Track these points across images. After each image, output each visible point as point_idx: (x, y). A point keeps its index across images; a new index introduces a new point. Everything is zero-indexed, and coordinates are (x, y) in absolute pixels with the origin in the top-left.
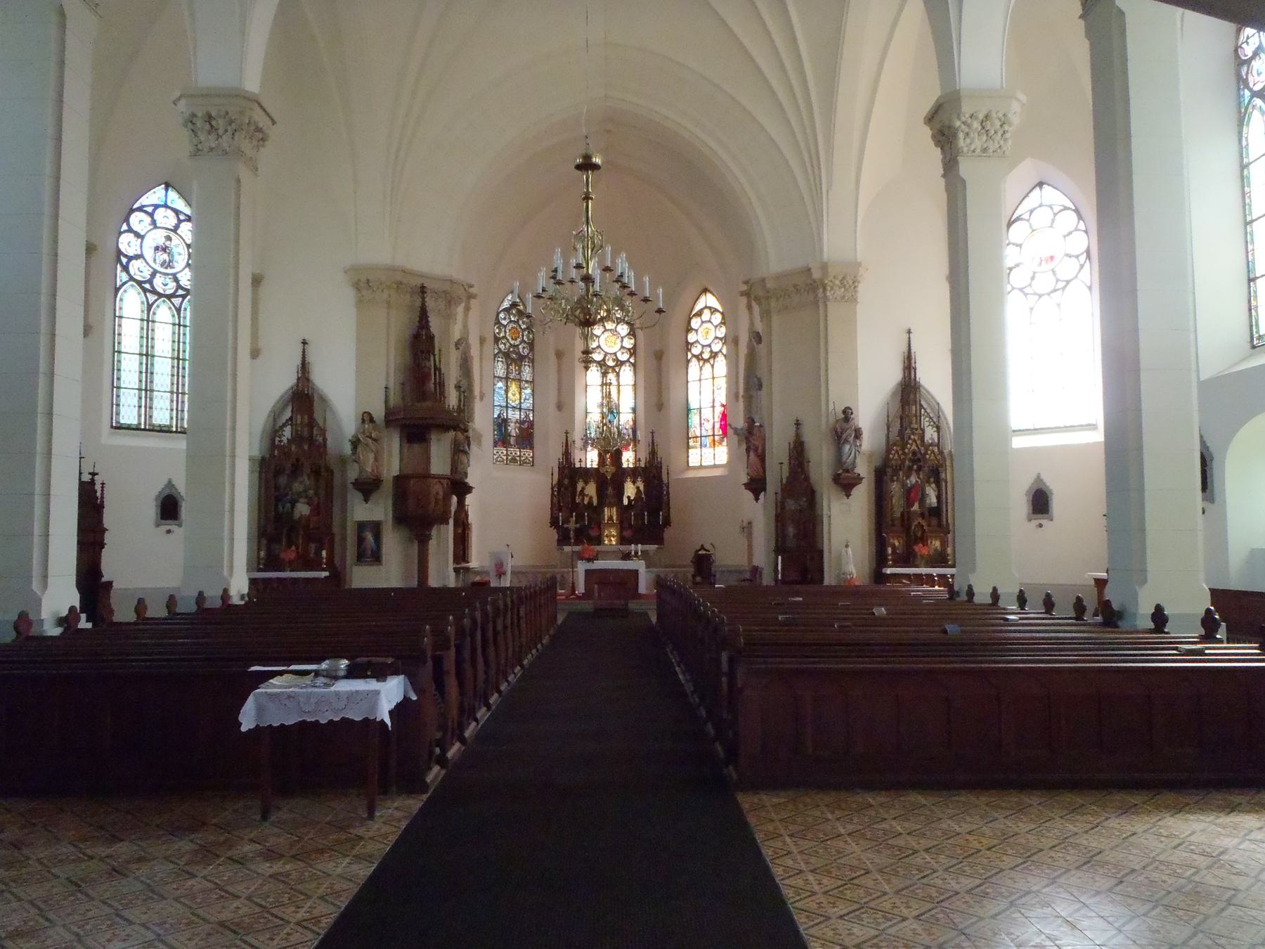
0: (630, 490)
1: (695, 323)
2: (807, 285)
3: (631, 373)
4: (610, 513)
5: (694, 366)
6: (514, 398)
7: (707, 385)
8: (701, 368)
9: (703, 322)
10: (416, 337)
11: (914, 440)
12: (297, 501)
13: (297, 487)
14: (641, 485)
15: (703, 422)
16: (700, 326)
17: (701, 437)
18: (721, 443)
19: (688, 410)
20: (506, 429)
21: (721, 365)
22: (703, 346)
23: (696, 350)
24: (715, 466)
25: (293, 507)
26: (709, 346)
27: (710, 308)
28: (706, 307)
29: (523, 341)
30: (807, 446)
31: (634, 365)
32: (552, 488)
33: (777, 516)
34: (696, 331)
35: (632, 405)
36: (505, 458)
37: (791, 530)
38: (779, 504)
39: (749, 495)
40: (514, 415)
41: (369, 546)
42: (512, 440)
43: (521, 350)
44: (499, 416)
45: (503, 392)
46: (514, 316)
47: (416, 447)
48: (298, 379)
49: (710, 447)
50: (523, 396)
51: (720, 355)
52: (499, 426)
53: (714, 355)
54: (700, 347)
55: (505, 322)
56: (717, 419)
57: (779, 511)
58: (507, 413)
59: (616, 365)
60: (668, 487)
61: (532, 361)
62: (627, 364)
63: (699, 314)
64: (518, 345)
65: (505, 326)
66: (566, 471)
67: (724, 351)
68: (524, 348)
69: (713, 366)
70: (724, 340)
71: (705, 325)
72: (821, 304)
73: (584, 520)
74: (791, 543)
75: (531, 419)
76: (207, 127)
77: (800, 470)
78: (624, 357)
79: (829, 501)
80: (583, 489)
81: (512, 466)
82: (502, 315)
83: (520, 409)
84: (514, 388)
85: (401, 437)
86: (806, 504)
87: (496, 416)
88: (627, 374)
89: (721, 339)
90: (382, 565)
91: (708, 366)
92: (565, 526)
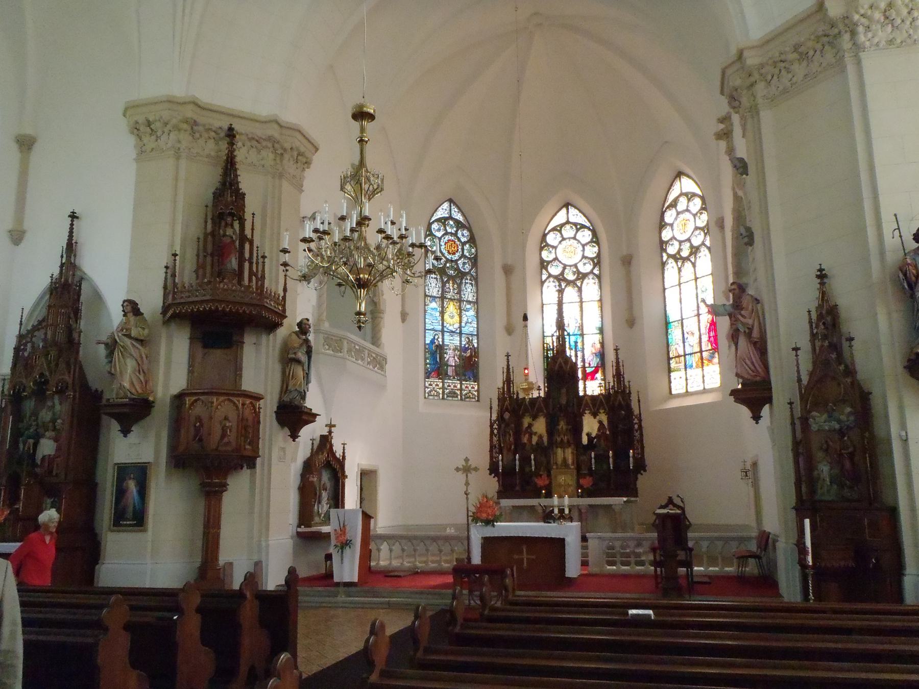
0: (590, 425)
1: (669, 216)
2: (818, 39)
3: (597, 287)
4: (563, 455)
5: (671, 268)
6: (452, 322)
7: (689, 289)
8: (680, 270)
9: (678, 213)
10: (218, 195)
12: (43, 436)
13: (45, 415)
14: (604, 418)
15: (686, 336)
16: (676, 219)
17: (685, 355)
18: (710, 361)
19: (667, 324)
20: (442, 358)
21: (705, 261)
22: (681, 242)
23: (672, 250)
24: (705, 391)
25: (36, 445)
26: (689, 240)
27: (686, 194)
28: (681, 194)
29: (463, 256)
30: (843, 313)
31: (599, 277)
32: (491, 426)
33: (796, 444)
34: (671, 225)
35: (599, 325)
36: (441, 391)
37: (824, 470)
38: (797, 422)
39: (744, 412)
40: (452, 342)
41: (130, 501)
42: (450, 371)
43: (461, 266)
44: (432, 342)
45: (438, 314)
46: (452, 227)
47: (218, 355)
48: (62, 265)
49: (697, 367)
50: (464, 319)
51: (703, 249)
52: (433, 354)
53: (695, 250)
54: (676, 244)
55: (439, 234)
56: (704, 330)
57: (799, 435)
58: (443, 339)
59: (577, 279)
60: (640, 420)
61: (476, 279)
62: (591, 276)
63: (674, 204)
64: (456, 261)
65: (440, 239)
66: (507, 403)
67: (708, 243)
68: (464, 264)
69: (694, 265)
70: (706, 230)
71: (682, 216)
73: (531, 467)
74: (827, 491)
75: (476, 345)
76: (148, 130)
77: (834, 356)
78: (586, 268)
79: (901, 408)
80: (530, 426)
81: (455, 402)
82: (435, 226)
83: (461, 334)
84: (451, 308)
85: (192, 339)
86: (852, 418)
87: (428, 342)
88: (591, 288)
89: (702, 229)
90: (145, 531)
91: (688, 265)
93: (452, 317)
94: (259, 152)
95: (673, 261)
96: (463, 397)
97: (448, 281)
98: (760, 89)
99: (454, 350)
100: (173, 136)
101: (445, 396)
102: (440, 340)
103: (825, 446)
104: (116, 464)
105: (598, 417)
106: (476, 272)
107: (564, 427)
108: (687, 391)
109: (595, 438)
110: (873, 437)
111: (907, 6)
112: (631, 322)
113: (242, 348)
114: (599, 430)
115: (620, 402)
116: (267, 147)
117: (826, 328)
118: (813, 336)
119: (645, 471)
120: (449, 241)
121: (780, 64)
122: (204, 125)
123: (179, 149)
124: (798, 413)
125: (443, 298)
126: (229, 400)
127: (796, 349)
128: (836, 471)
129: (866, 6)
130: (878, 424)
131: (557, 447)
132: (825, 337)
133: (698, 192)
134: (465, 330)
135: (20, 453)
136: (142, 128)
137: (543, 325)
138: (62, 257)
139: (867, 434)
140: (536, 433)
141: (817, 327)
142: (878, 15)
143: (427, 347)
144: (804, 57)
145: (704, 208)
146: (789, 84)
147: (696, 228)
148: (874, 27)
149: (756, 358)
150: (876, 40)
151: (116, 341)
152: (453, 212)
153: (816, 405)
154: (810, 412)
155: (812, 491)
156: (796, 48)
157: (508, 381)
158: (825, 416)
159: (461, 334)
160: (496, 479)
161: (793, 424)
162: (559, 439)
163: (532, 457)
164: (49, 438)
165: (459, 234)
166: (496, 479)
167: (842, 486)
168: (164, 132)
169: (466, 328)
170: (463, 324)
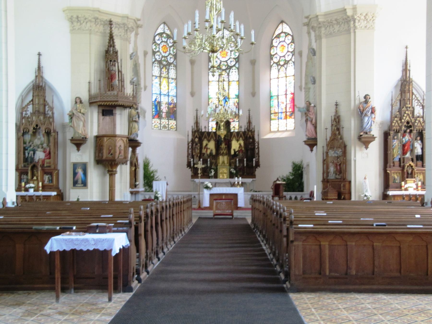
0: (235, 145)
4: (223, 159)
6: (164, 90)
8: (279, 70)
11: (408, 114)
13: (37, 142)
14: (242, 142)
15: (280, 103)
20: (160, 108)
21: (291, 69)
23: (275, 60)
24: (286, 130)
27: (285, 33)
30: (342, 118)
31: (238, 69)
32: (188, 144)
33: (324, 161)
37: (332, 169)
39: (308, 148)
40: (164, 100)
42: (164, 115)
44: (156, 100)
46: (165, 38)
47: (108, 118)
49: (284, 119)
51: (291, 62)
52: (156, 106)
53: (286, 62)
55: (159, 42)
56: (288, 102)
57: (325, 158)
61: (176, 66)
62: (234, 68)
63: (278, 36)
64: (167, 57)
65: (159, 45)
67: (293, 60)
70: (293, 53)
72: (352, 31)
76: (76, 20)
80: (207, 145)
83: (168, 96)
84: (164, 82)
85: (389, 191)
86: (341, 153)
87: (154, 100)
88: (234, 75)
90: (87, 188)
91: (283, 68)
92: (409, 125)
93: (165, 87)
94: (118, 29)
95: (276, 65)
96: (169, 128)
97: (163, 68)
98: (323, 29)
99: (166, 104)
100: (89, 24)
101: (161, 128)
102: (159, 99)
103: (332, 162)
104: (72, 163)
105: (239, 142)
106: (176, 63)
107: (224, 147)
108: (278, 130)
109: (237, 151)
110: (346, 160)
111: (372, 15)
112: (254, 94)
113: (116, 115)
114: (239, 148)
115: (250, 136)
116: (122, 27)
117: (336, 123)
118: (332, 125)
119: (259, 167)
120: (164, 45)
121: (330, 24)
122: (100, 19)
123: (91, 30)
124: (325, 150)
125: (160, 77)
126: (122, 139)
127: (326, 129)
128: (335, 170)
129: (359, 14)
130: (348, 155)
131: (220, 155)
132: (336, 126)
133: (290, 33)
134: (170, 94)
135: (26, 157)
136: (74, 19)
137: (209, 92)
138: (36, 72)
139: (345, 158)
140: (209, 149)
141: (334, 122)
142: (362, 17)
143: (153, 102)
144: (338, 23)
145: (293, 41)
146: (332, 32)
147: (288, 51)
148: (361, 21)
149: (313, 129)
150: (361, 26)
151: (73, 114)
152: (165, 30)
153: (331, 148)
154: (328, 150)
155: (328, 176)
156: (336, 20)
157: (197, 123)
158: (333, 152)
159: (168, 96)
160: (190, 169)
161: (323, 154)
162: (222, 152)
163: (209, 160)
164: (41, 151)
165: (168, 42)
166: (190, 169)
167: (336, 174)
168: (84, 22)
169: (171, 92)
170: (170, 91)
